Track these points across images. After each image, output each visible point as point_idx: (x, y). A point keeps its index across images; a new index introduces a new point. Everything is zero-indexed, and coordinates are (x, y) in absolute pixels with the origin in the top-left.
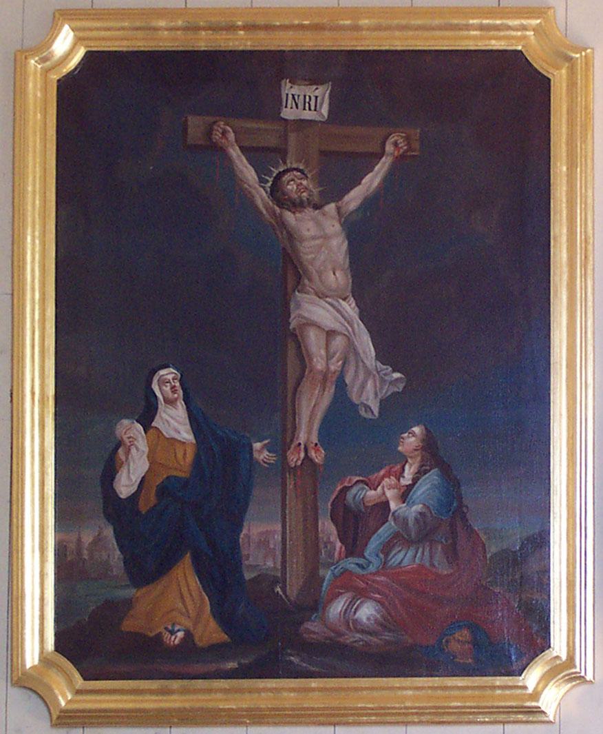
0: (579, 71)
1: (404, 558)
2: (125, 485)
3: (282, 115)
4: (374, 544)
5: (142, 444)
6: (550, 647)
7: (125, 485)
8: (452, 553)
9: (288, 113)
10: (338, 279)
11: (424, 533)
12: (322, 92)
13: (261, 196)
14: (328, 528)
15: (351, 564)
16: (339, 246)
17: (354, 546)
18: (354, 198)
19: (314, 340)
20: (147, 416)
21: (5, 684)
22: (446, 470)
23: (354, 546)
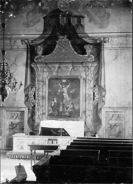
0: (24, 166)
1: (70, 110)
2: (53, 105)
3: (27, 179)
4: (68, 109)
5: (53, 103)
6: (13, 150)
7: (53, 105)
8: (73, 110)
9: (63, 82)
10: (66, 92)
11: (72, 109)
12: (65, 80)
13: (61, 87)
14: (65, 108)
15: (67, 110)
16: (66, 90)
17: (67, 109)
18: (67, 87)
19: (64, 96)
20: (54, 101)
21: (22, 48)
22: (73, 105)
23: (67, 109)
